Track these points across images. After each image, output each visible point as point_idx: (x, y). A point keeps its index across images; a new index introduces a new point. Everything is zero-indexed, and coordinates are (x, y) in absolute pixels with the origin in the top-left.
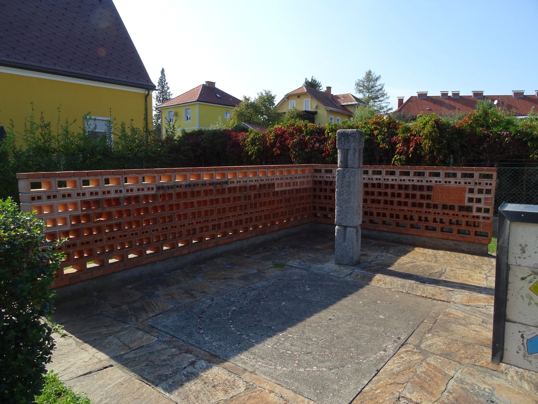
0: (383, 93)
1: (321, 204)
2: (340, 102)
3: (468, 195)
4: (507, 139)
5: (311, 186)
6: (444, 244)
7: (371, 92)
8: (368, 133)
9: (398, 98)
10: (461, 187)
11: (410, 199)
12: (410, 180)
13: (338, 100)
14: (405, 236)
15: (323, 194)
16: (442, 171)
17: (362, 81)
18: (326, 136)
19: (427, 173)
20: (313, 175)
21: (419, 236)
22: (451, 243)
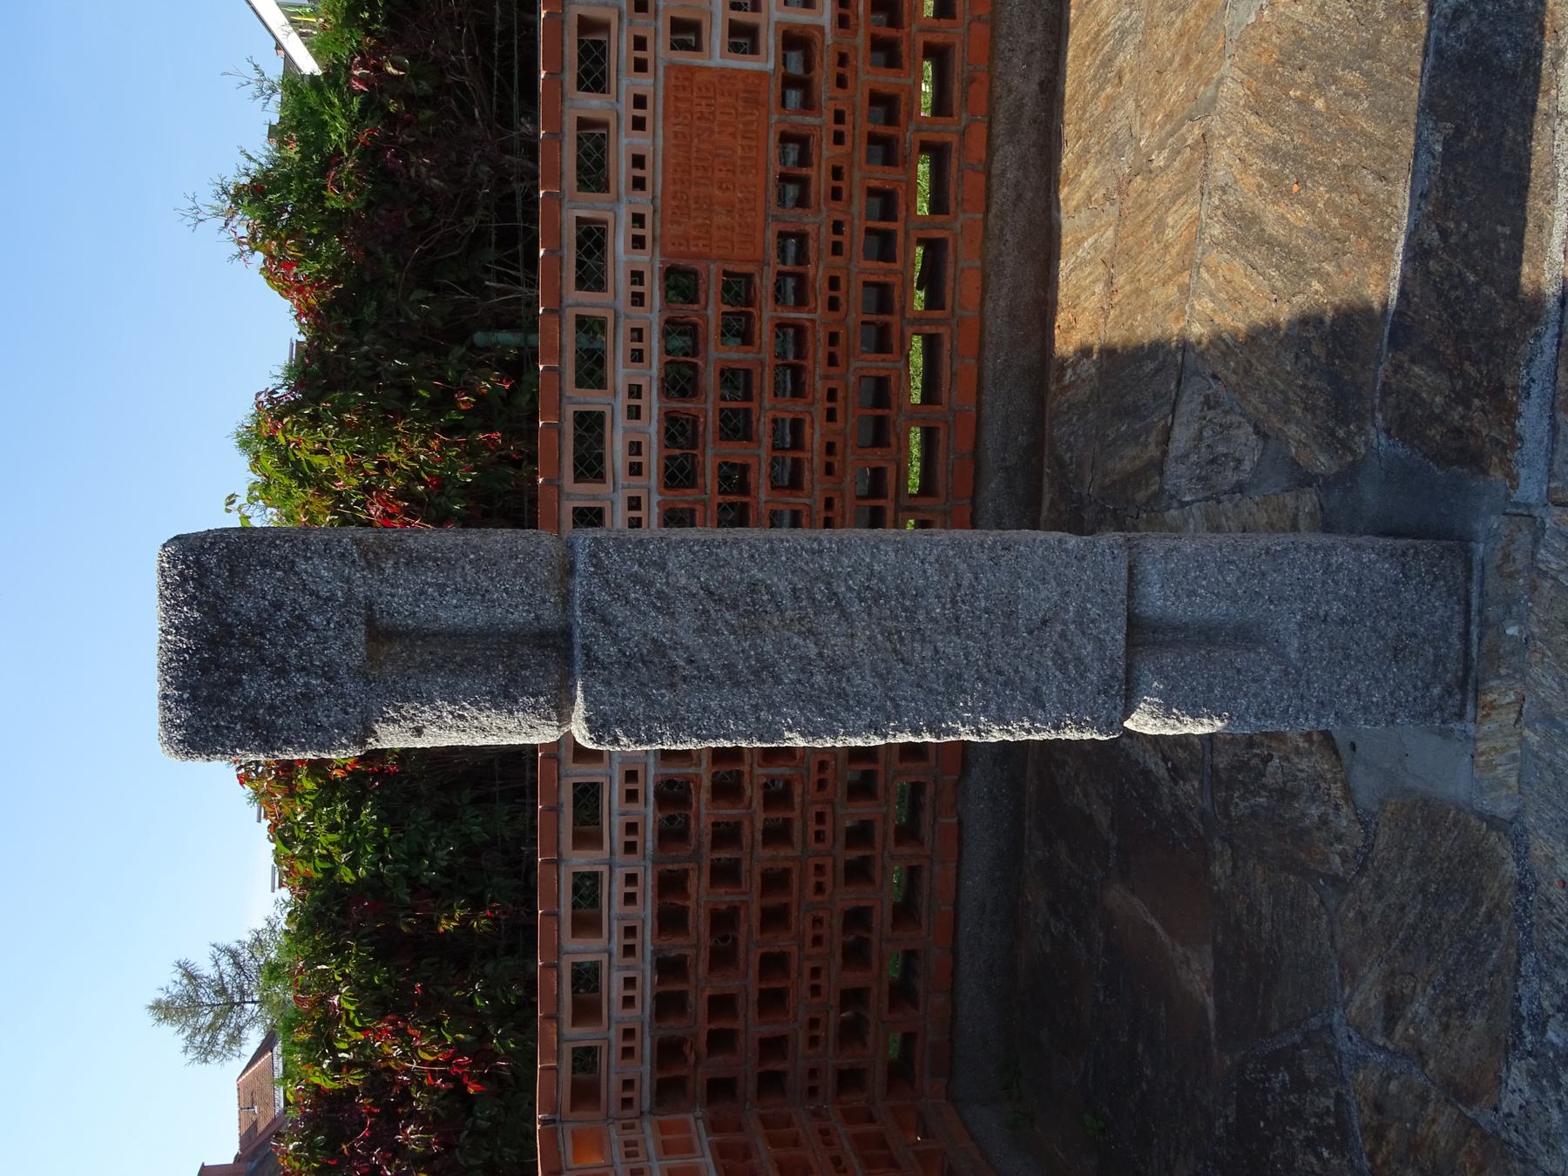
0: (251, 946)
1: (820, 1033)
2: (269, 1120)
3: (716, 54)
4: (390, 69)
5: (695, 1121)
6: (1020, 197)
7: (243, 993)
8: (343, 813)
9: (277, 890)
10: (666, 97)
11: (753, 405)
12: (634, 413)
13: (261, 1127)
14: (992, 436)
15: (751, 1026)
16: (566, 205)
17: (191, 1037)
18: (355, 1079)
19: (579, 301)
20: (615, 1108)
21: (981, 346)
22: (1008, 159)
